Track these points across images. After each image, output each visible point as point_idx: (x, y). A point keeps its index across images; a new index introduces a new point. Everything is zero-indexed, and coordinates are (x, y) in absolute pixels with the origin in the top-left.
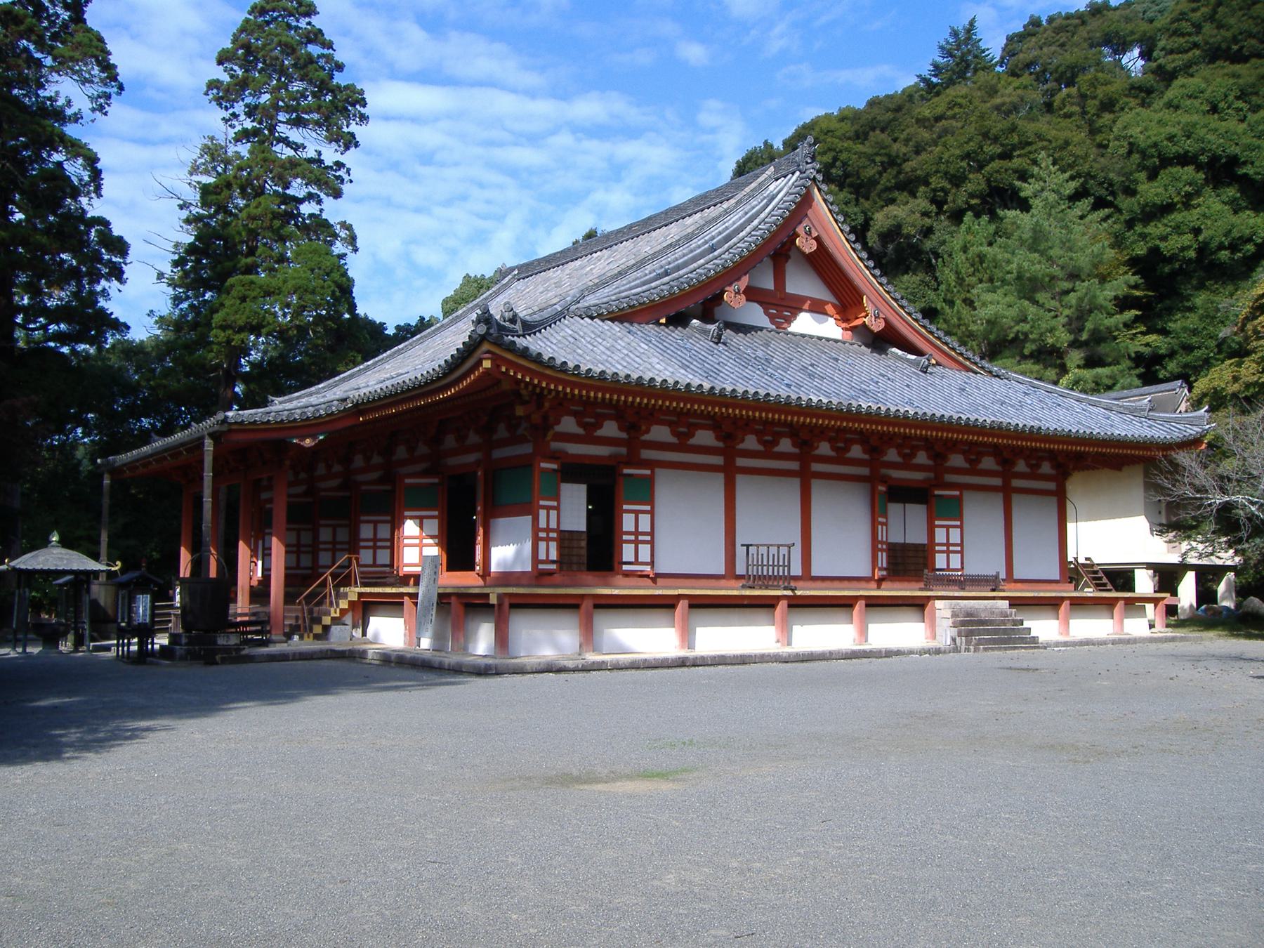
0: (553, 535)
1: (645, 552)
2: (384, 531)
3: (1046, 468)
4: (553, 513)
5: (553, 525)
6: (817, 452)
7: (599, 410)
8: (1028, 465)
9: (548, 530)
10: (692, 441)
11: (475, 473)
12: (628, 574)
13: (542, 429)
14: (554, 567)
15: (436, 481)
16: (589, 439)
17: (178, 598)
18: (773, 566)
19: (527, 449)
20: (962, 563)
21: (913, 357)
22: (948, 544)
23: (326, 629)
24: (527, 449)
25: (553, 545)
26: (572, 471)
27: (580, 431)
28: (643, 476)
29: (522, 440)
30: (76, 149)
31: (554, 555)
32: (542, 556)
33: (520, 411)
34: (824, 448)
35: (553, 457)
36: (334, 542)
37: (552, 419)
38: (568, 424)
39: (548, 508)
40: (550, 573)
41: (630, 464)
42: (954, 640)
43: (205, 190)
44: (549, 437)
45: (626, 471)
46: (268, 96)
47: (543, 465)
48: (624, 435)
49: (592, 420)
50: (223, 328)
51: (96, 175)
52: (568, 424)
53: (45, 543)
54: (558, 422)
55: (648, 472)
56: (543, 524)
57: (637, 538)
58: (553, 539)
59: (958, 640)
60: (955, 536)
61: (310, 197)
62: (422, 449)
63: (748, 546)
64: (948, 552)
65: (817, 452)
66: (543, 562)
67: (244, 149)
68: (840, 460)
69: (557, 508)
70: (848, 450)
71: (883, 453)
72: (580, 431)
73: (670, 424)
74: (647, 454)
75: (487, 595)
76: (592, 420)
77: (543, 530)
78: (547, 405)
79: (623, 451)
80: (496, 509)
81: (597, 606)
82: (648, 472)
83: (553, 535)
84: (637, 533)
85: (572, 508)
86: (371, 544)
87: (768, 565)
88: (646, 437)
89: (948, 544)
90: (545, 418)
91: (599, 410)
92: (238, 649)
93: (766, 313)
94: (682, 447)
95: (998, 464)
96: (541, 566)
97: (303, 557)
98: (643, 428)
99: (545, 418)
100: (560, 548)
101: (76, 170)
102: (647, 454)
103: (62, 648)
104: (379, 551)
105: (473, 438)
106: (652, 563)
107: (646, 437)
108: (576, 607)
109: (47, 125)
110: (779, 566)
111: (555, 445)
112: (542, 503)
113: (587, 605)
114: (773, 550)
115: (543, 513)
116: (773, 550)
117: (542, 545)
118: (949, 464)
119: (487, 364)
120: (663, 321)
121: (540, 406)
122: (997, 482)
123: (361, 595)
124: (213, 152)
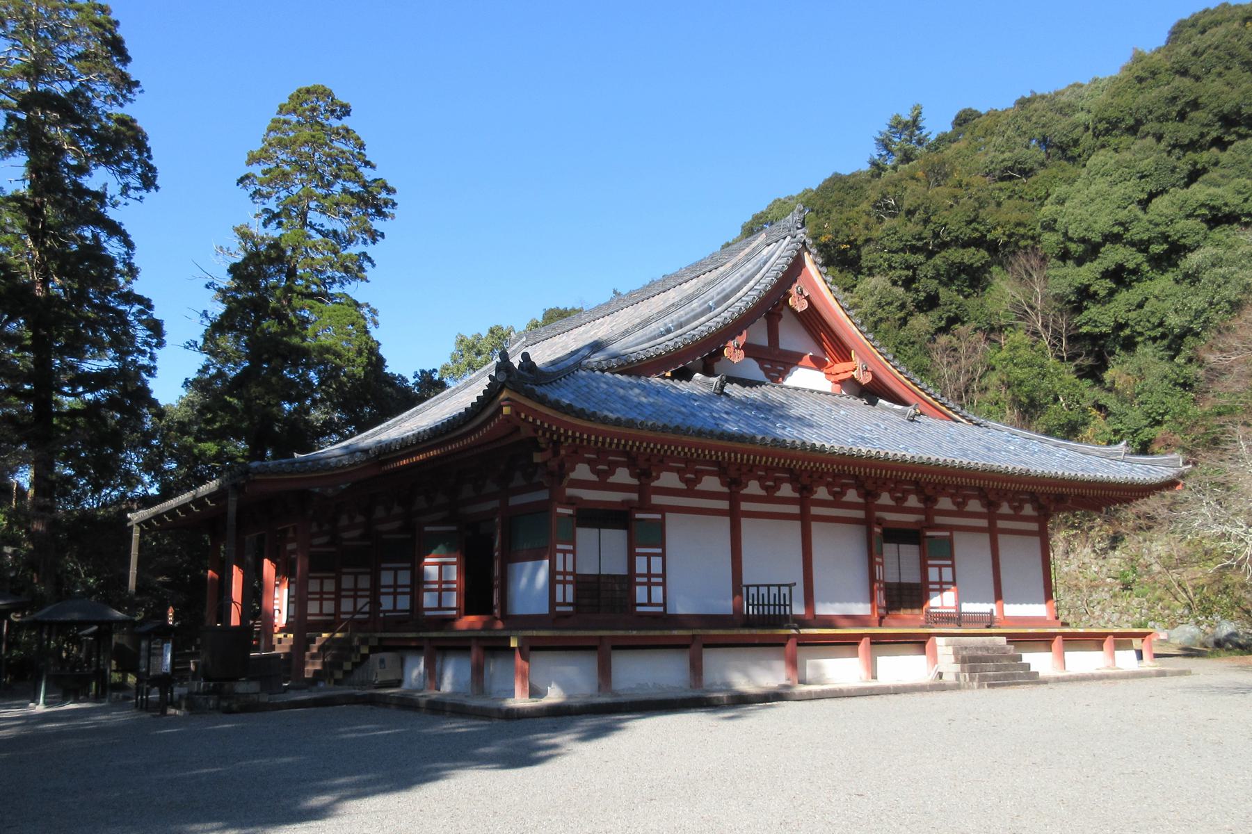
0: (570, 578)
1: (657, 593)
3: (1028, 510)
4: (570, 557)
5: (570, 568)
6: (815, 496)
9: (565, 573)
10: (699, 487)
13: (559, 475)
14: (570, 609)
15: (454, 528)
18: (763, 605)
19: (543, 495)
21: (900, 407)
24: (543, 495)
25: (570, 588)
27: (683, 486)
29: (540, 487)
30: (114, 229)
32: (559, 598)
34: (822, 493)
37: (567, 465)
38: (582, 472)
39: (565, 552)
42: (957, 677)
44: (565, 482)
47: (559, 510)
49: (606, 468)
54: (573, 469)
55: (659, 516)
56: (560, 568)
58: (569, 582)
65: (815, 496)
68: (837, 503)
69: (573, 552)
73: (678, 470)
74: (657, 499)
76: (606, 468)
77: (560, 573)
78: (563, 452)
79: (635, 496)
80: (512, 556)
82: (659, 516)
83: (570, 578)
87: (780, 605)
88: (655, 484)
90: (561, 466)
93: (762, 368)
94: (690, 492)
96: (558, 609)
101: (113, 248)
102: (657, 499)
104: (399, 597)
111: (570, 492)
112: (559, 547)
114: (774, 590)
115: (560, 557)
116: (763, 590)
117: (559, 588)
121: (556, 453)
123: (380, 639)
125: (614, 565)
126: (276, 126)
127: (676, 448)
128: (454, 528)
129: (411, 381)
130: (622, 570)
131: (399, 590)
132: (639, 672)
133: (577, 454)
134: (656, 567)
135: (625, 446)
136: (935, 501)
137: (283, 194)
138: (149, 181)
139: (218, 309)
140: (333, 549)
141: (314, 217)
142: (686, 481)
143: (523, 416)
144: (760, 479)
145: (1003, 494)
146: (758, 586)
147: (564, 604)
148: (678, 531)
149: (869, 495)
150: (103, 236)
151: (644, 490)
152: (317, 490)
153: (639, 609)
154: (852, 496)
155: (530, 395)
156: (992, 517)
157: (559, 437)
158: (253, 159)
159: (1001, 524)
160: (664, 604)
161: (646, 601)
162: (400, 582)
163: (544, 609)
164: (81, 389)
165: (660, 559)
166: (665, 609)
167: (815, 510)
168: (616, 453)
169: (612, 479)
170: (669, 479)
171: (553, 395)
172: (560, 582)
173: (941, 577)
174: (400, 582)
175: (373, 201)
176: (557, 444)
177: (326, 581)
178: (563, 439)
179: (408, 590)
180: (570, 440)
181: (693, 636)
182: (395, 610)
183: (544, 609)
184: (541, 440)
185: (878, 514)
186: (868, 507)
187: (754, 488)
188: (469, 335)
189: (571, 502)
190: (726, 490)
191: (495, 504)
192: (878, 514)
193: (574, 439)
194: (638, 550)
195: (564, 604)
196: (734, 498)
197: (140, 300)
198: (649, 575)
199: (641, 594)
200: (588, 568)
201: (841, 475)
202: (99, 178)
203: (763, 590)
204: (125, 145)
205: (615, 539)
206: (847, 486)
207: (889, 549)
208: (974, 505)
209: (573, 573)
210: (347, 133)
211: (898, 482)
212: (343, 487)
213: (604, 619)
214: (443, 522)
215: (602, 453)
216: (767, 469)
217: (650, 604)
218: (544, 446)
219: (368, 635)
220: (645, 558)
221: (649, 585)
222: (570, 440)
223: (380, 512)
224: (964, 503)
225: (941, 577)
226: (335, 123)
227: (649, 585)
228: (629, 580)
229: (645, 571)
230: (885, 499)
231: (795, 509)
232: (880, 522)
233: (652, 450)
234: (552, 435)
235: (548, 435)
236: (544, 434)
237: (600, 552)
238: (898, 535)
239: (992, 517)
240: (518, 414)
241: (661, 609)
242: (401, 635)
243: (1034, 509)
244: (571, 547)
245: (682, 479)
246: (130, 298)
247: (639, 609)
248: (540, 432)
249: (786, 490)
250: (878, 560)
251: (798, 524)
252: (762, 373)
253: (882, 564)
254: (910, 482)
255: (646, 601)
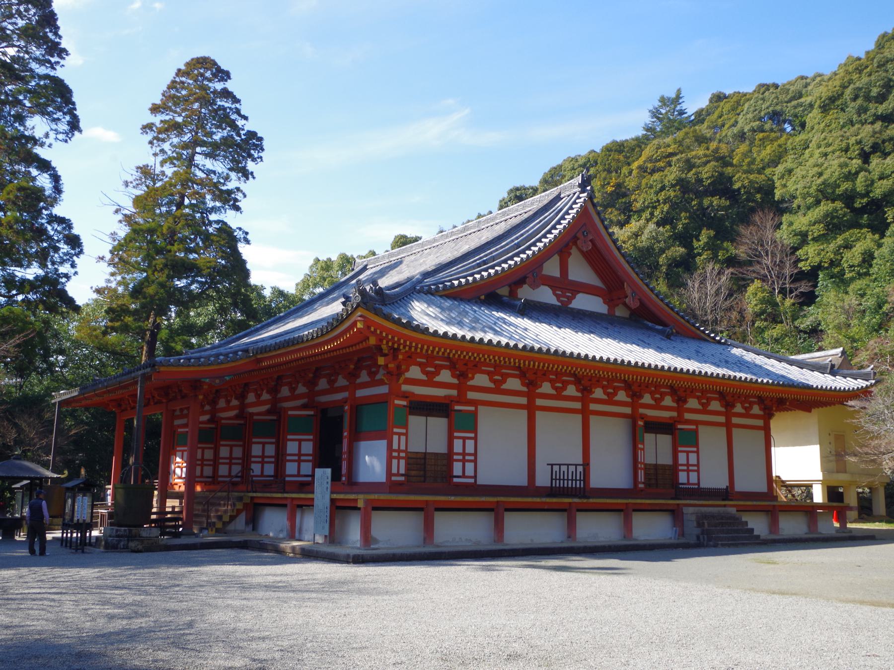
0: (403, 455)
1: (470, 467)
3: (756, 410)
4: (403, 438)
5: (403, 447)
6: (593, 396)
7: (437, 362)
8: (744, 407)
9: (399, 451)
10: (504, 386)
11: (343, 407)
13: (396, 374)
14: (402, 478)
15: (312, 413)
17: (109, 498)
18: (572, 480)
19: (383, 390)
20: (699, 479)
21: (661, 327)
22: (688, 465)
24: (383, 390)
25: (402, 462)
27: (424, 377)
28: (471, 411)
29: (381, 383)
30: (45, 166)
31: (402, 471)
32: (394, 471)
33: (381, 361)
34: (598, 393)
36: (231, 458)
37: (403, 367)
38: (415, 372)
39: (399, 434)
42: (698, 538)
43: (137, 201)
44: (401, 380)
45: (457, 408)
46: (189, 135)
47: (397, 402)
49: (433, 369)
51: (58, 190)
52: (415, 372)
54: (407, 370)
55: (473, 408)
56: (395, 447)
57: (464, 458)
58: (403, 458)
59: (701, 537)
60: (693, 459)
62: (301, 389)
63: (552, 465)
64: (688, 471)
65: (593, 396)
66: (395, 475)
67: (169, 170)
68: (610, 401)
69: (406, 434)
70: (615, 394)
71: (641, 397)
72: (424, 377)
73: (488, 373)
74: (471, 395)
75: (356, 500)
76: (433, 369)
77: (395, 451)
78: (400, 357)
79: (454, 392)
80: (357, 436)
82: (473, 408)
83: (403, 455)
86: (266, 460)
87: (568, 480)
88: (470, 383)
89: (688, 465)
90: (399, 367)
91: (437, 362)
93: (554, 294)
94: (498, 390)
95: (722, 406)
96: (394, 478)
97: (205, 468)
98: (470, 375)
99: (399, 367)
101: (44, 181)
102: (471, 395)
103: (17, 538)
104: (302, 464)
105: (342, 382)
107: (470, 383)
108: (285, 506)
109: (24, 150)
110: (576, 480)
111: (405, 388)
112: (395, 430)
114: (572, 468)
115: (395, 438)
116: (564, 468)
117: (395, 462)
118: (687, 406)
119: (359, 325)
120: (483, 297)
121: (395, 357)
122: (722, 419)
123: (252, 498)
124: (145, 171)
125: (438, 446)
126: (173, 85)
127: (473, 354)
128: (312, 413)
129: (267, 293)
130: (442, 449)
131: (266, 460)
132: (453, 529)
133: (411, 358)
134: (470, 448)
135: (449, 354)
136: (685, 402)
137: (176, 140)
138: (74, 125)
139: (123, 231)
140: (213, 426)
141: (199, 159)
142: (608, 394)
143: (372, 329)
144: (551, 381)
145: (596, 381)
146: (560, 465)
147: (398, 474)
148: (487, 419)
149: (635, 395)
150: (34, 172)
151: (462, 388)
152: (207, 380)
153: (455, 480)
154: (622, 396)
155: (377, 312)
156: (728, 415)
157: (399, 345)
158: (155, 109)
159: (735, 420)
160: (475, 477)
161: (461, 474)
162: (234, 455)
163: (382, 478)
164: (14, 292)
165: (472, 442)
166: (476, 481)
167: (539, 402)
168: (439, 359)
169: (437, 379)
170: (481, 380)
171: (386, 310)
172: (395, 457)
173: (262, 467)
174: (234, 455)
175: (244, 148)
176: (395, 351)
177: (206, 451)
178: (401, 347)
179: (273, 460)
180: (407, 348)
181: (498, 502)
182: (262, 475)
183: (382, 478)
184: (384, 347)
185: (641, 411)
186: (634, 405)
187: (546, 388)
188: (323, 258)
189: (405, 396)
190: (579, 394)
191: (346, 394)
192: (641, 411)
193: (410, 347)
194: (456, 434)
195: (398, 474)
196: (531, 395)
197: (62, 221)
198: (464, 454)
199: (457, 468)
200: (416, 446)
201: (615, 379)
202: (37, 125)
203: (564, 468)
204: (58, 97)
205: (438, 425)
206: (665, 394)
207: (649, 438)
208: (715, 405)
209: (406, 451)
210: (227, 94)
211: (658, 386)
212: (227, 378)
213: (430, 486)
214: (304, 407)
215: (430, 358)
216: (556, 373)
217: (464, 476)
218: (386, 352)
219: (242, 494)
220: (461, 441)
221: (464, 461)
222: (407, 348)
223: (251, 398)
224: (708, 404)
225: (262, 467)
226: (219, 86)
227: (464, 461)
228: (449, 457)
229: (461, 451)
230: (647, 399)
231: (578, 405)
232: (642, 417)
233: (459, 356)
234: (393, 344)
235: (390, 344)
236: (387, 343)
237: (427, 435)
238: (656, 427)
239: (728, 415)
240: (369, 328)
241: (472, 481)
242: (268, 495)
243: (761, 409)
244: (404, 431)
245: (491, 380)
246: (53, 219)
247: (455, 480)
248: (385, 342)
249: (571, 390)
250: (640, 446)
251: (580, 417)
252: (554, 298)
253: (643, 449)
254: (667, 387)
255: (461, 474)
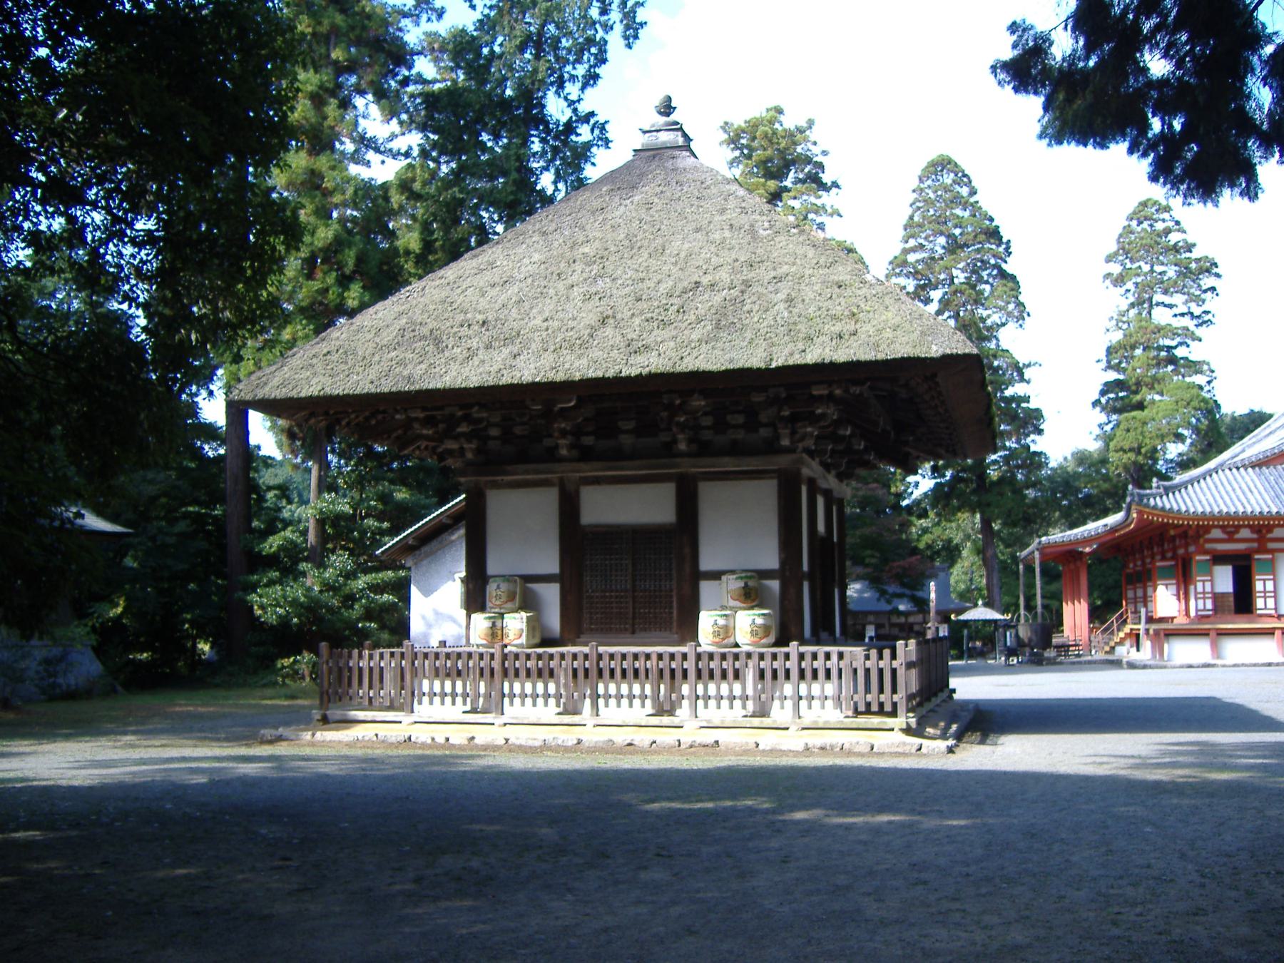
2: (1140, 593)
12: (1261, 616)
16: (1231, 539)
23: (1113, 648)
26: (1219, 559)
35: (1206, 552)
38: (1217, 533)
40: (1208, 616)
41: (1258, 551)
48: (1255, 536)
50: (1117, 451)
53: (976, 605)
61: (1181, 344)
74: (1271, 545)
79: (1255, 545)
81: (1219, 634)
84: (1204, 598)
85: (1224, 580)
92: (1055, 658)
100: (1214, 603)
102: (1271, 545)
106: (1276, 609)
111: (1208, 546)
113: (1213, 634)
158: (1109, 259)
